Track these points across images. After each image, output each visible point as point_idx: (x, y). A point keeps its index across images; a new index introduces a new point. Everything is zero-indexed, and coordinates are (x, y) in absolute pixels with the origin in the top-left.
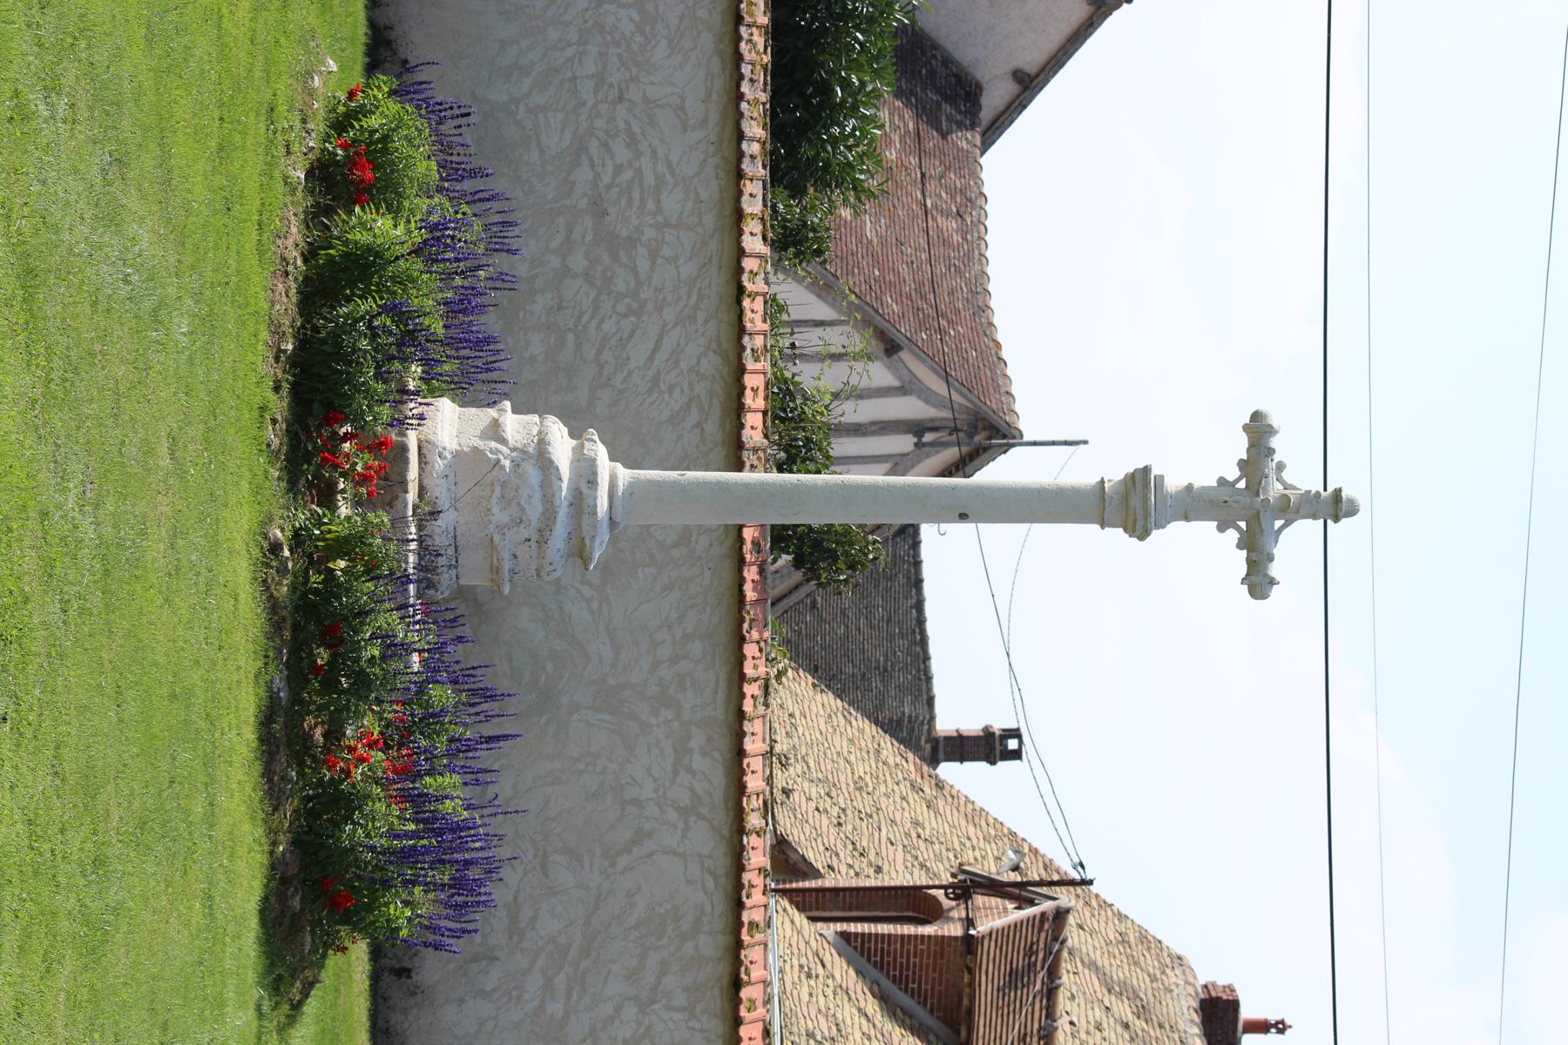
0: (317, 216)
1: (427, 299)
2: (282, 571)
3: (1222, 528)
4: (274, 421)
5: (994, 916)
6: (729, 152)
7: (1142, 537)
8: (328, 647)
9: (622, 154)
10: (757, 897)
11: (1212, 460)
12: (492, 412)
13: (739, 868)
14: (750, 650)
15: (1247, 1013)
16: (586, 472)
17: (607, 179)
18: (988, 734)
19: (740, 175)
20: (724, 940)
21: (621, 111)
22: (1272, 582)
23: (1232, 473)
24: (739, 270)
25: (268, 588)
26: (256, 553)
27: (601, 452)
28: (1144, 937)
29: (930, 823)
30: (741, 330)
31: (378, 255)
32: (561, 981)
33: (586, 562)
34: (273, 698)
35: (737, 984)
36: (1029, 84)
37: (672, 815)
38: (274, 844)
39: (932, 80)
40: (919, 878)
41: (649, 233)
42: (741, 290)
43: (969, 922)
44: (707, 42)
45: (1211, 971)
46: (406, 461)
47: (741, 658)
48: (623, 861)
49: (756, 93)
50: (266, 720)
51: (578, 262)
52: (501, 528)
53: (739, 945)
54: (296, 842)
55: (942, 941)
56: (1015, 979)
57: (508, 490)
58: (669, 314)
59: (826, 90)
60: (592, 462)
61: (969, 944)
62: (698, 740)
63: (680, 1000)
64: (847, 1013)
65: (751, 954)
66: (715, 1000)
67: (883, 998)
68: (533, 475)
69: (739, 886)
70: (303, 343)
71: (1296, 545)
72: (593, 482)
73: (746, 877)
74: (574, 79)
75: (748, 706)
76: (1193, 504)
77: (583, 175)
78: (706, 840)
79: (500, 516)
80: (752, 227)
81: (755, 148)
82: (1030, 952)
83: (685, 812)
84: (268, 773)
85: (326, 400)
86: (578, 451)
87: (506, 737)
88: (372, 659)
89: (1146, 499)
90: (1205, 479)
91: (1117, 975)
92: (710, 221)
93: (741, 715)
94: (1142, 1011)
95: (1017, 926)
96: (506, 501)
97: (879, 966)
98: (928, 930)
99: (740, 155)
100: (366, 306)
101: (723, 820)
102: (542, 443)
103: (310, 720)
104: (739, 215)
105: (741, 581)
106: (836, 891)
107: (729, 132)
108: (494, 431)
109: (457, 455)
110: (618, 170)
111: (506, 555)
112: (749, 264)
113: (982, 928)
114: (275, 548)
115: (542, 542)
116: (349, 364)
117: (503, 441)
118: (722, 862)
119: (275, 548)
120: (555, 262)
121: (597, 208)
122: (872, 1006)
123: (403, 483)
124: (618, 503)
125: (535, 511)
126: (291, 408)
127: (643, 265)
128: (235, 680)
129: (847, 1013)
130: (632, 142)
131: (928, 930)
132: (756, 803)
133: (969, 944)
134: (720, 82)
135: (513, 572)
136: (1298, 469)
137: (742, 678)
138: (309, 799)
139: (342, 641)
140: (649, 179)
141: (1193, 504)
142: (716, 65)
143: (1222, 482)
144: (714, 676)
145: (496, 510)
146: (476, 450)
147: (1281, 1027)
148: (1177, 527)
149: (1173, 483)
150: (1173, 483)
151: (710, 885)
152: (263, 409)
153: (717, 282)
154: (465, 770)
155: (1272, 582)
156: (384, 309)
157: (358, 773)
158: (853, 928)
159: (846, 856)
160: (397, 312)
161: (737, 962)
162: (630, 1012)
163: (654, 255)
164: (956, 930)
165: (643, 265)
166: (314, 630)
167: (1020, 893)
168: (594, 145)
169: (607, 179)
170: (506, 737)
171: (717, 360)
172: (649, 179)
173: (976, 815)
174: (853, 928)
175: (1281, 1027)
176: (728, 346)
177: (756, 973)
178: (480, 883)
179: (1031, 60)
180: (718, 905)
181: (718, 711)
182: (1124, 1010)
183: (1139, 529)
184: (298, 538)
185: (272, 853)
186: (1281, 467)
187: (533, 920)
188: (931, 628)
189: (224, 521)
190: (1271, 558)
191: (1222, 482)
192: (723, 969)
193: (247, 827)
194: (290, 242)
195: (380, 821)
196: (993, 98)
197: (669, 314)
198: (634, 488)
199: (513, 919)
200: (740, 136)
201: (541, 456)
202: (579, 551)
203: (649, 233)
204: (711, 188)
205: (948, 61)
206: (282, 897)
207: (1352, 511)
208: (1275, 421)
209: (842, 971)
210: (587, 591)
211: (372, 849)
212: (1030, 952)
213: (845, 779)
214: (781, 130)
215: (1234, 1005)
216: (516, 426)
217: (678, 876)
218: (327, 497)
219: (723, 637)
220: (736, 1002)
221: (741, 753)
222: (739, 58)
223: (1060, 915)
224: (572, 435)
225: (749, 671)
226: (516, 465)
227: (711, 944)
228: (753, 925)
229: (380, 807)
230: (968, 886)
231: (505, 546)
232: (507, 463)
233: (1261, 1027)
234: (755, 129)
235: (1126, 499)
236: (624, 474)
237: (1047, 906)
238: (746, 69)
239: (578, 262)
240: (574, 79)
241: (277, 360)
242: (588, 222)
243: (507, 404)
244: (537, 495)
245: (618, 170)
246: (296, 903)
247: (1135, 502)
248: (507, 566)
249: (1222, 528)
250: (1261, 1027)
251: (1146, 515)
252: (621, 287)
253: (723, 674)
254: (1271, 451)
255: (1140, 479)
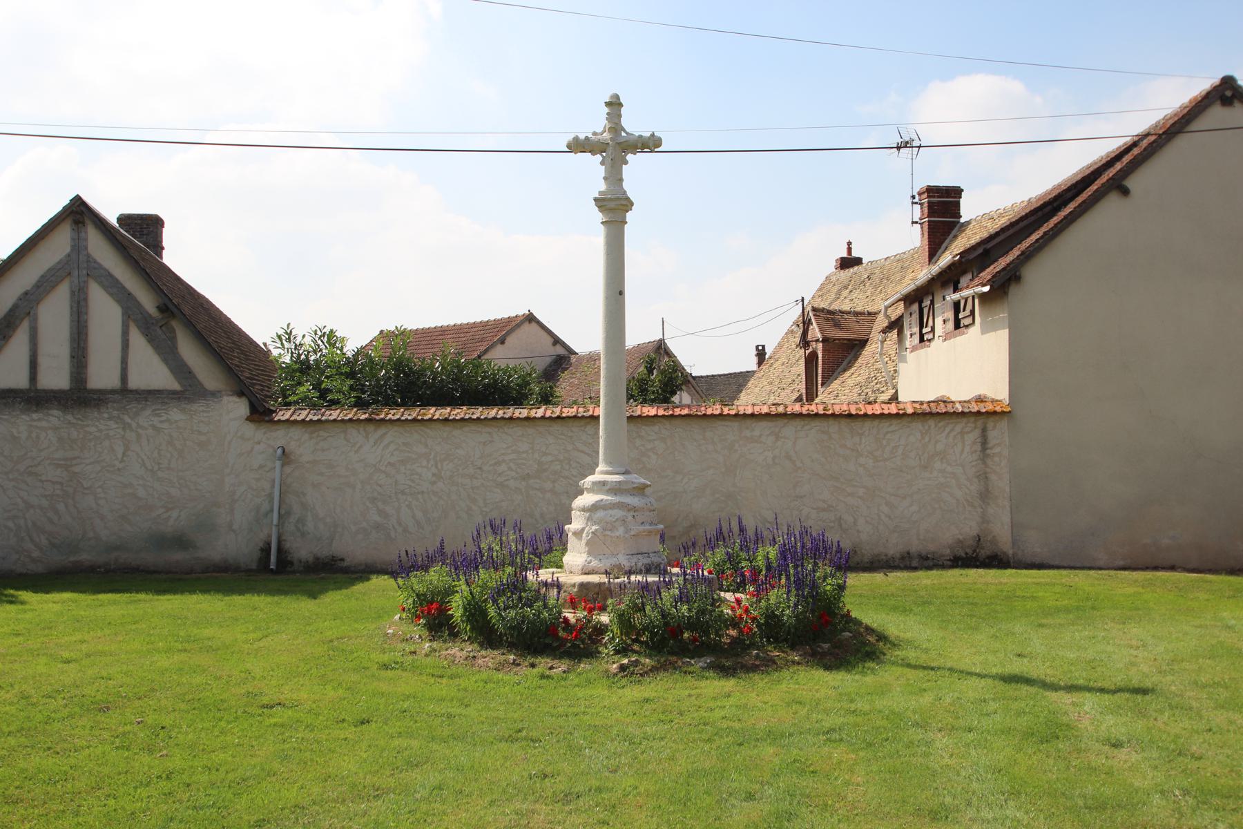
0: (454, 635)
1: (487, 577)
2: (637, 663)
3: (626, 163)
4: (551, 668)
5: (815, 332)
6: (503, 423)
7: (632, 204)
8: (682, 633)
9: (503, 467)
10: (813, 407)
11: (592, 167)
12: (570, 535)
13: (800, 415)
14: (709, 412)
15: (845, 255)
16: (600, 486)
17: (514, 474)
18: (758, 355)
19: (511, 418)
20: (831, 421)
21: (485, 468)
22: (653, 135)
23: (598, 158)
24: (550, 418)
25: (646, 673)
26: (624, 681)
27: (590, 479)
28: (820, 290)
29: (783, 359)
30: (575, 417)
31: (469, 604)
32: (849, 490)
33: (646, 486)
34: (710, 667)
35: (850, 416)
36: (557, 341)
37: (779, 443)
38: (793, 662)
39: (556, 371)
40: (802, 362)
41: (536, 456)
42: (558, 417)
43: (817, 341)
44: (457, 432)
45: (830, 267)
46: (588, 583)
47: (713, 416)
48: (799, 464)
49: (478, 412)
50: (726, 671)
51: (548, 485)
52: (627, 531)
53: (833, 415)
54: (793, 647)
55: (824, 350)
56: (837, 325)
57: (607, 527)
58: (570, 447)
59: (486, 387)
60: (594, 483)
61: (825, 341)
62: (747, 433)
63: (857, 439)
64: (850, 382)
65: (837, 410)
66: (857, 425)
67: (845, 370)
68: (600, 514)
69: (808, 415)
70: (512, 646)
71: (634, 124)
72: (604, 483)
73: (805, 412)
74: (473, 488)
75: (733, 412)
76: (614, 176)
77: (512, 483)
78: (790, 429)
79: (620, 531)
80: (533, 413)
81: (501, 412)
82: (827, 319)
83: (778, 438)
84: (753, 669)
85: (544, 638)
86: (590, 490)
87: (740, 523)
88: (690, 610)
89: (611, 199)
90: (601, 171)
91: (833, 296)
92: (530, 431)
93: (736, 415)
94: (845, 287)
95: (818, 324)
96: (613, 528)
97: (833, 372)
98: (820, 356)
99: (503, 418)
100: (492, 612)
101: (780, 422)
102: (584, 510)
103: (725, 640)
104: (527, 418)
105: (680, 416)
106: (807, 389)
107: (493, 423)
108: (578, 534)
109: (589, 553)
110: (510, 469)
111: (642, 528)
112: (548, 414)
113: (819, 336)
114: (623, 668)
115: (634, 509)
116: (523, 622)
117: (583, 529)
118: (798, 422)
119: (623, 668)
120: (548, 495)
121: (526, 477)
122: (848, 373)
123: (600, 585)
124: (618, 470)
125: (618, 513)
126: (548, 656)
127: (550, 458)
128: (705, 693)
129: (850, 382)
130: (498, 463)
131: (820, 356)
132: (773, 408)
133: (825, 341)
134: (473, 427)
135: (651, 524)
136: (595, 123)
137: (721, 415)
138: (768, 641)
139: (679, 625)
140: (513, 456)
141: (614, 176)
142: (466, 429)
143: (602, 163)
144: (720, 426)
145: (618, 534)
146: (587, 544)
147: (849, 243)
148: (626, 185)
149: (603, 186)
150: (603, 186)
151: (807, 427)
152: (543, 677)
153: (556, 427)
154: (756, 542)
155: (653, 135)
156: (495, 602)
157: (755, 613)
158: (820, 382)
159: (794, 386)
160: (500, 592)
161: (841, 416)
162: (862, 460)
163: (545, 454)
164: (820, 346)
165: (550, 458)
166: (679, 640)
167: (806, 324)
168: (499, 479)
169: (514, 474)
170: (740, 523)
171: (589, 427)
172: (513, 456)
173: (780, 346)
174: (820, 382)
175: (849, 243)
176: (583, 422)
177: (845, 408)
178: (813, 540)
179: (550, 340)
180: (816, 423)
181: (735, 424)
182: (845, 293)
183: (627, 204)
184: (622, 651)
185: (799, 663)
186: (595, 134)
187: (824, 501)
188: (726, 372)
189: (604, 699)
190: (641, 136)
191: (602, 163)
192: (844, 422)
193: (783, 686)
194: (458, 654)
195: (780, 598)
196: (560, 350)
197: (570, 447)
198: (608, 462)
199: (824, 510)
200: (495, 418)
201: (594, 508)
202: (640, 490)
203: (536, 456)
204: (517, 430)
205: (550, 366)
206: (823, 655)
207: (617, 97)
208: (571, 137)
209: (835, 385)
210: (686, 480)
211: (796, 605)
212: (827, 319)
213: (768, 388)
214: (504, 402)
215: (842, 259)
216: (577, 523)
217: (804, 440)
218: (601, 630)
219: (704, 423)
220: (857, 416)
221: (752, 415)
222: (462, 419)
223: (814, 309)
224: (582, 493)
225: (718, 412)
226: (595, 523)
227: (833, 426)
228: (825, 409)
229: (773, 600)
230: (805, 343)
231: (636, 529)
232: (594, 528)
233: (849, 250)
234: (493, 412)
235: (611, 210)
236: (602, 467)
237: (811, 314)
238: (467, 416)
239: (548, 485)
240: (473, 488)
241: (518, 665)
242: (531, 481)
243: (566, 527)
244: (610, 512)
245: (510, 469)
246: (826, 646)
247: (612, 205)
248: (648, 527)
249: (626, 163)
250: (849, 250)
251: (618, 199)
252: (559, 467)
253: (719, 423)
254: (587, 138)
255: (601, 202)
